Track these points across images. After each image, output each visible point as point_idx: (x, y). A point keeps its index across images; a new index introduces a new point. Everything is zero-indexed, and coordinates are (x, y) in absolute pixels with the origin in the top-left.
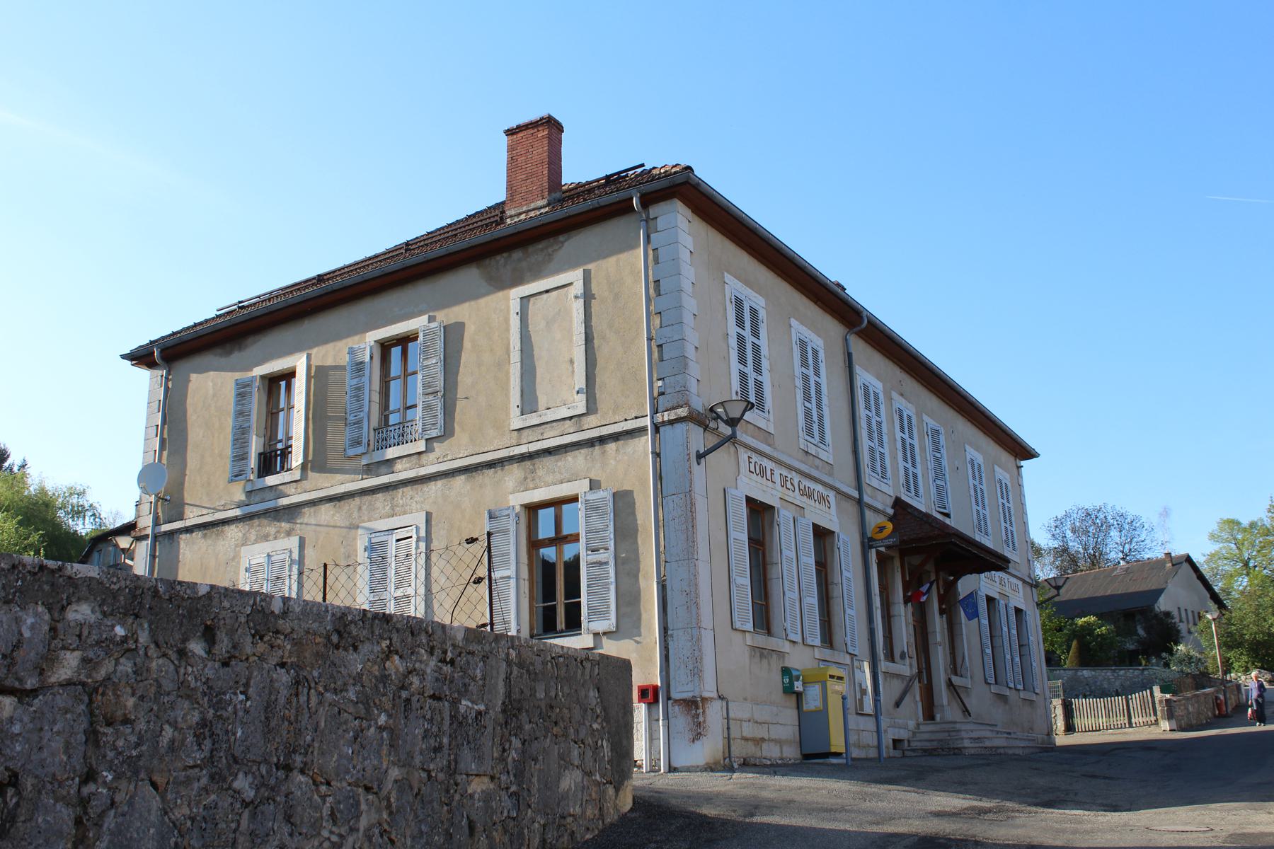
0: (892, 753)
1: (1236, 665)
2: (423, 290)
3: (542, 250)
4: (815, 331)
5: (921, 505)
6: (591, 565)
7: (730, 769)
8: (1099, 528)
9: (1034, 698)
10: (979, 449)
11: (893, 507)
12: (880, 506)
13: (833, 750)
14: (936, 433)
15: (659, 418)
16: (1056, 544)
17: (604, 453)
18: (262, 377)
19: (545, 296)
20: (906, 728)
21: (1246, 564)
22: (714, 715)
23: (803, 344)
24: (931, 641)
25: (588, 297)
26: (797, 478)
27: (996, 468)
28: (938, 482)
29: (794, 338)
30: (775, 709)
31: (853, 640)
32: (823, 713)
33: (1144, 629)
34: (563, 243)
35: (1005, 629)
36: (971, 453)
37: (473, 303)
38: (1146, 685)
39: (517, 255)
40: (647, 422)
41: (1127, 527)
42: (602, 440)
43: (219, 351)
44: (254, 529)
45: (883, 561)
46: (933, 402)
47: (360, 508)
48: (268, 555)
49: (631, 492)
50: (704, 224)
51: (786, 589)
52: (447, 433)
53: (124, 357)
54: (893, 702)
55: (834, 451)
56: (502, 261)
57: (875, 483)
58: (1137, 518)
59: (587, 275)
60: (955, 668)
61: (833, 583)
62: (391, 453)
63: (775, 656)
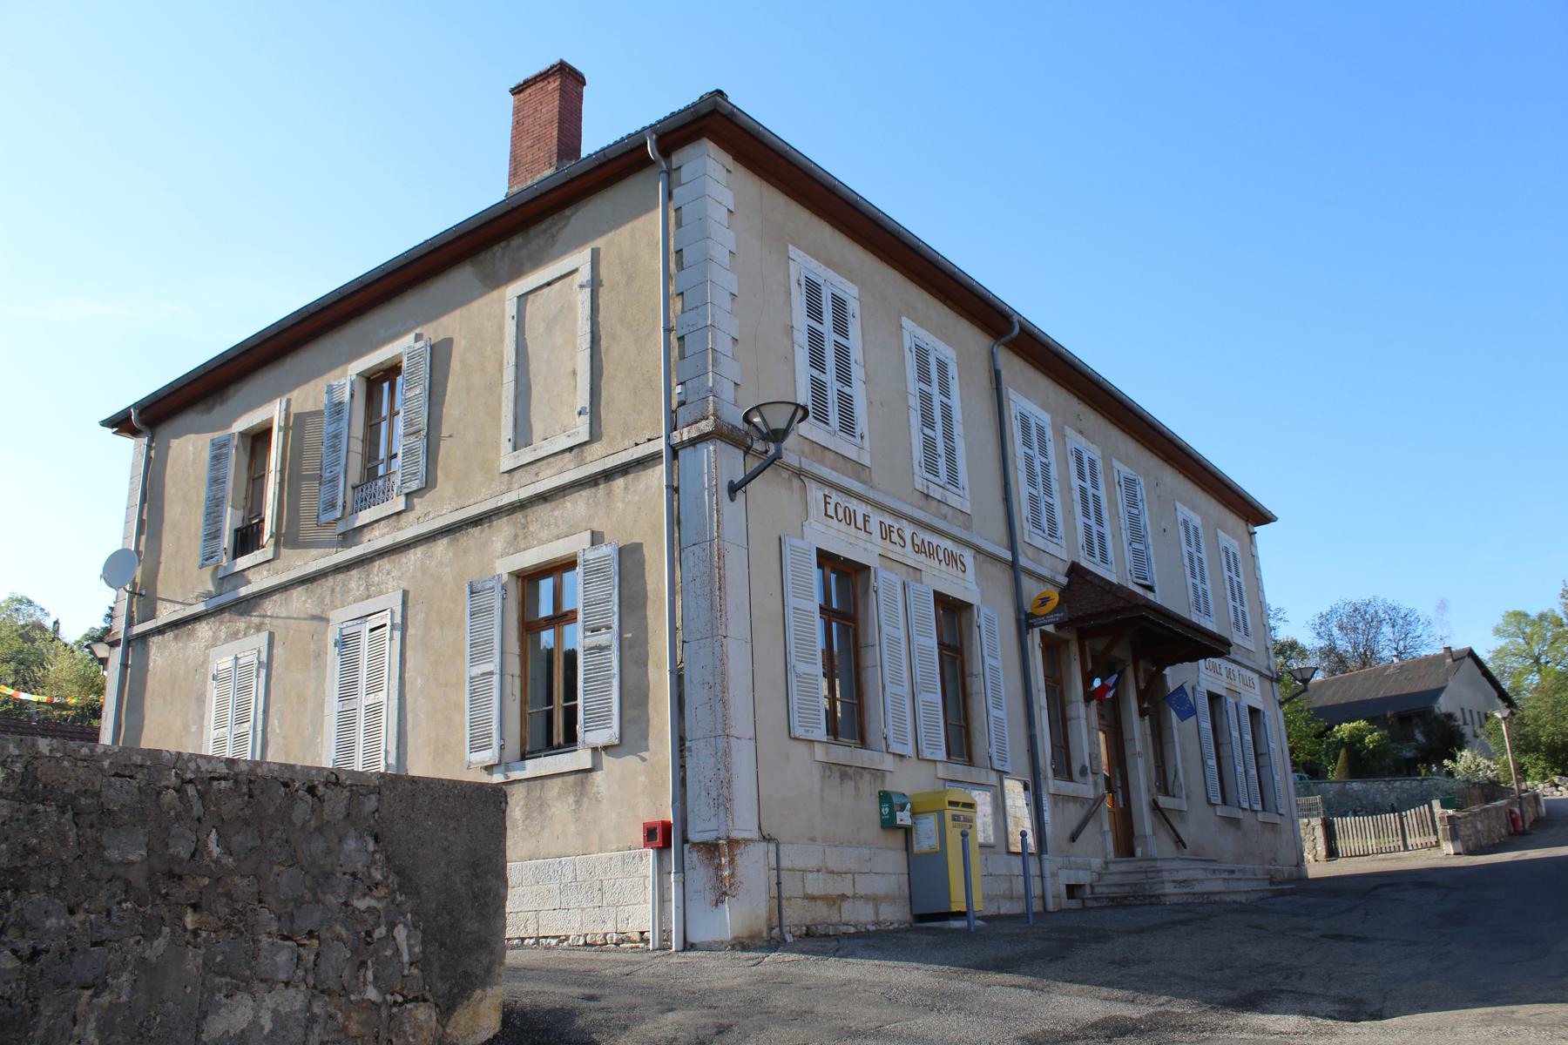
0: (1066, 903)
1: (1532, 772)
3: (545, 231)
5: (1113, 572)
6: (590, 650)
7: (774, 944)
8: (1368, 624)
9: (1278, 820)
10: (1194, 508)
11: (1067, 575)
12: (1045, 573)
13: (954, 908)
14: (1130, 483)
15: (676, 437)
16: (1323, 643)
17: (609, 493)
18: (243, 434)
19: (546, 290)
20: (1087, 868)
21: (1537, 661)
22: (753, 866)
23: (922, 354)
24: (1128, 752)
25: (595, 284)
26: (908, 530)
27: (1221, 534)
28: (1135, 545)
29: (907, 342)
30: (867, 852)
31: (1002, 752)
32: (940, 855)
33: (1423, 733)
34: (569, 218)
35: (1235, 734)
36: (1184, 512)
38: (1426, 800)
39: (516, 241)
40: (661, 445)
42: (608, 475)
43: (201, 407)
45: (1052, 648)
46: (1128, 446)
47: (333, 591)
48: (237, 658)
49: (639, 546)
50: (756, 178)
51: (887, 681)
52: (430, 483)
53: (108, 423)
54: (1068, 833)
55: (973, 493)
56: (498, 254)
57: (1039, 542)
59: (595, 254)
60: (1163, 782)
61: (971, 674)
62: (365, 517)
63: (867, 776)
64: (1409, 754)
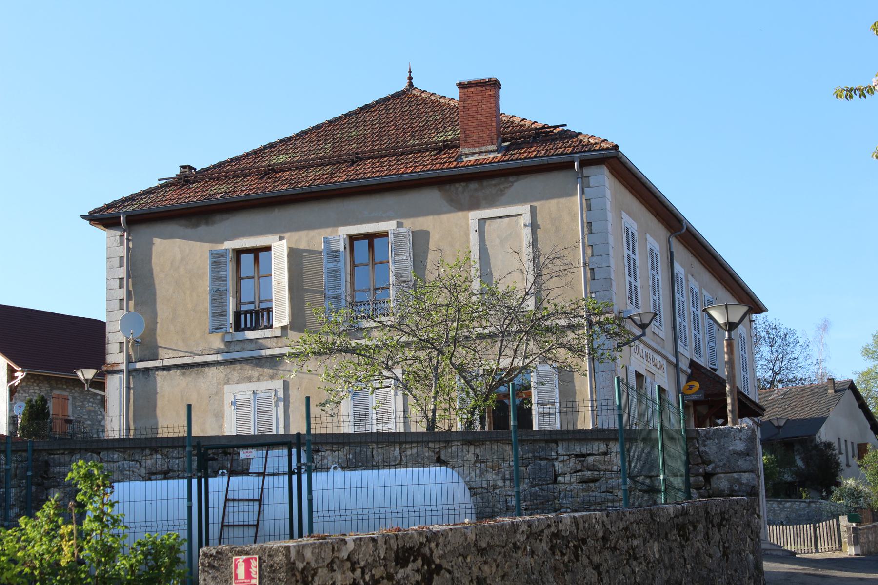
2: (390, 200)
3: (495, 185)
4: (655, 239)
5: (702, 362)
11: (690, 367)
19: (499, 220)
25: (534, 227)
28: (711, 344)
33: (803, 459)
34: (513, 183)
37: (436, 217)
39: (473, 186)
41: (779, 342)
44: (235, 372)
56: (460, 189)
58: (793, 332)
59: (533, 211)
64: (788, 478)
